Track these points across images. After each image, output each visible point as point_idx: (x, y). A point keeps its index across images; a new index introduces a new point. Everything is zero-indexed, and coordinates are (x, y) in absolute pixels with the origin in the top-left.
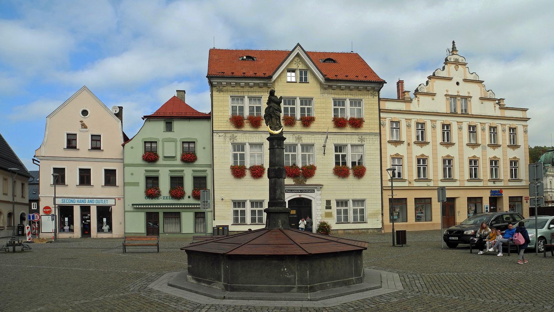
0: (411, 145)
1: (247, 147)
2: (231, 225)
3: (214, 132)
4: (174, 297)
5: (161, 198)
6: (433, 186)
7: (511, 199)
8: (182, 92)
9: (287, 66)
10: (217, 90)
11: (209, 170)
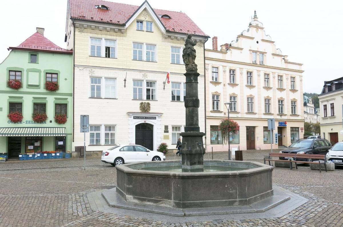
0: (226, 86)
1: (103, 81)
2: (88, 146)
3: (75, 66)
5: (24, 122)
6: (240, 117)
7: (292, 129)
9: (137, 17)
10: (79, 31)
11: (70, 99)
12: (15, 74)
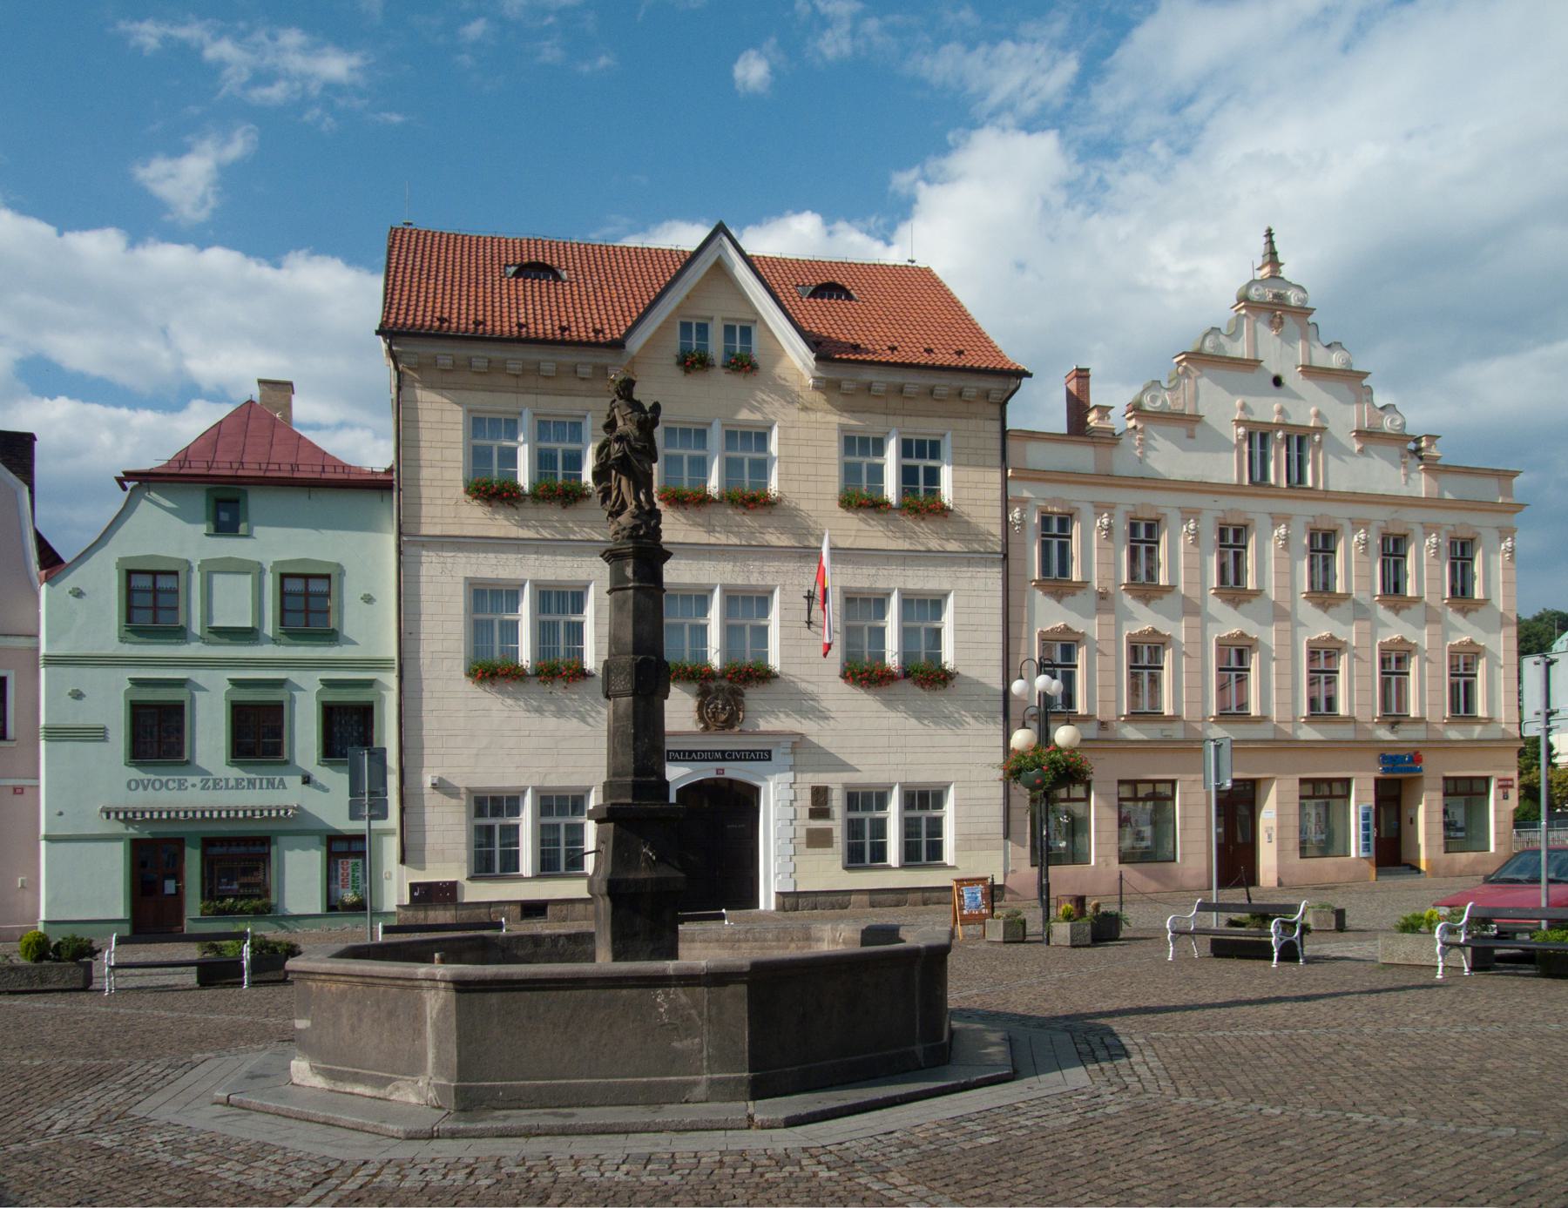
4: (238, 1144)
8: (279, 389)
9: (679, 308)
12: (154, 583)
